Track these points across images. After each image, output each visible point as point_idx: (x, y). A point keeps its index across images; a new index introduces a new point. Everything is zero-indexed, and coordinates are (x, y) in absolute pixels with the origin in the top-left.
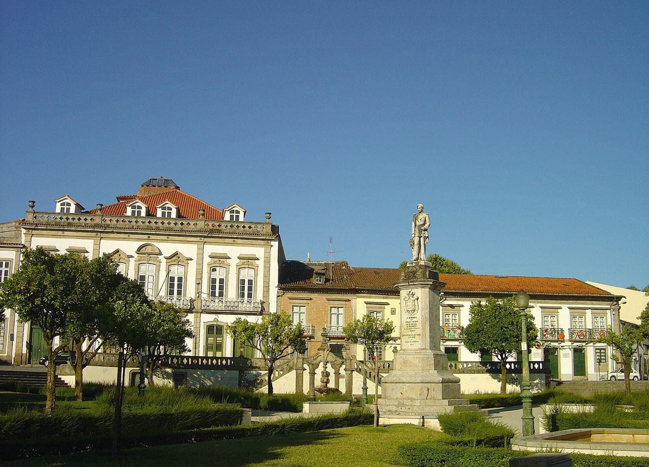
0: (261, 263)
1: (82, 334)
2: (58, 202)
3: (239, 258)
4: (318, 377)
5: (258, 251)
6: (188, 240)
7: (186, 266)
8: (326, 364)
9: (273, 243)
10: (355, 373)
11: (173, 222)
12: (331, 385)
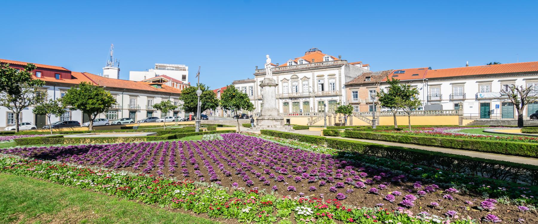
0: (337, 76)
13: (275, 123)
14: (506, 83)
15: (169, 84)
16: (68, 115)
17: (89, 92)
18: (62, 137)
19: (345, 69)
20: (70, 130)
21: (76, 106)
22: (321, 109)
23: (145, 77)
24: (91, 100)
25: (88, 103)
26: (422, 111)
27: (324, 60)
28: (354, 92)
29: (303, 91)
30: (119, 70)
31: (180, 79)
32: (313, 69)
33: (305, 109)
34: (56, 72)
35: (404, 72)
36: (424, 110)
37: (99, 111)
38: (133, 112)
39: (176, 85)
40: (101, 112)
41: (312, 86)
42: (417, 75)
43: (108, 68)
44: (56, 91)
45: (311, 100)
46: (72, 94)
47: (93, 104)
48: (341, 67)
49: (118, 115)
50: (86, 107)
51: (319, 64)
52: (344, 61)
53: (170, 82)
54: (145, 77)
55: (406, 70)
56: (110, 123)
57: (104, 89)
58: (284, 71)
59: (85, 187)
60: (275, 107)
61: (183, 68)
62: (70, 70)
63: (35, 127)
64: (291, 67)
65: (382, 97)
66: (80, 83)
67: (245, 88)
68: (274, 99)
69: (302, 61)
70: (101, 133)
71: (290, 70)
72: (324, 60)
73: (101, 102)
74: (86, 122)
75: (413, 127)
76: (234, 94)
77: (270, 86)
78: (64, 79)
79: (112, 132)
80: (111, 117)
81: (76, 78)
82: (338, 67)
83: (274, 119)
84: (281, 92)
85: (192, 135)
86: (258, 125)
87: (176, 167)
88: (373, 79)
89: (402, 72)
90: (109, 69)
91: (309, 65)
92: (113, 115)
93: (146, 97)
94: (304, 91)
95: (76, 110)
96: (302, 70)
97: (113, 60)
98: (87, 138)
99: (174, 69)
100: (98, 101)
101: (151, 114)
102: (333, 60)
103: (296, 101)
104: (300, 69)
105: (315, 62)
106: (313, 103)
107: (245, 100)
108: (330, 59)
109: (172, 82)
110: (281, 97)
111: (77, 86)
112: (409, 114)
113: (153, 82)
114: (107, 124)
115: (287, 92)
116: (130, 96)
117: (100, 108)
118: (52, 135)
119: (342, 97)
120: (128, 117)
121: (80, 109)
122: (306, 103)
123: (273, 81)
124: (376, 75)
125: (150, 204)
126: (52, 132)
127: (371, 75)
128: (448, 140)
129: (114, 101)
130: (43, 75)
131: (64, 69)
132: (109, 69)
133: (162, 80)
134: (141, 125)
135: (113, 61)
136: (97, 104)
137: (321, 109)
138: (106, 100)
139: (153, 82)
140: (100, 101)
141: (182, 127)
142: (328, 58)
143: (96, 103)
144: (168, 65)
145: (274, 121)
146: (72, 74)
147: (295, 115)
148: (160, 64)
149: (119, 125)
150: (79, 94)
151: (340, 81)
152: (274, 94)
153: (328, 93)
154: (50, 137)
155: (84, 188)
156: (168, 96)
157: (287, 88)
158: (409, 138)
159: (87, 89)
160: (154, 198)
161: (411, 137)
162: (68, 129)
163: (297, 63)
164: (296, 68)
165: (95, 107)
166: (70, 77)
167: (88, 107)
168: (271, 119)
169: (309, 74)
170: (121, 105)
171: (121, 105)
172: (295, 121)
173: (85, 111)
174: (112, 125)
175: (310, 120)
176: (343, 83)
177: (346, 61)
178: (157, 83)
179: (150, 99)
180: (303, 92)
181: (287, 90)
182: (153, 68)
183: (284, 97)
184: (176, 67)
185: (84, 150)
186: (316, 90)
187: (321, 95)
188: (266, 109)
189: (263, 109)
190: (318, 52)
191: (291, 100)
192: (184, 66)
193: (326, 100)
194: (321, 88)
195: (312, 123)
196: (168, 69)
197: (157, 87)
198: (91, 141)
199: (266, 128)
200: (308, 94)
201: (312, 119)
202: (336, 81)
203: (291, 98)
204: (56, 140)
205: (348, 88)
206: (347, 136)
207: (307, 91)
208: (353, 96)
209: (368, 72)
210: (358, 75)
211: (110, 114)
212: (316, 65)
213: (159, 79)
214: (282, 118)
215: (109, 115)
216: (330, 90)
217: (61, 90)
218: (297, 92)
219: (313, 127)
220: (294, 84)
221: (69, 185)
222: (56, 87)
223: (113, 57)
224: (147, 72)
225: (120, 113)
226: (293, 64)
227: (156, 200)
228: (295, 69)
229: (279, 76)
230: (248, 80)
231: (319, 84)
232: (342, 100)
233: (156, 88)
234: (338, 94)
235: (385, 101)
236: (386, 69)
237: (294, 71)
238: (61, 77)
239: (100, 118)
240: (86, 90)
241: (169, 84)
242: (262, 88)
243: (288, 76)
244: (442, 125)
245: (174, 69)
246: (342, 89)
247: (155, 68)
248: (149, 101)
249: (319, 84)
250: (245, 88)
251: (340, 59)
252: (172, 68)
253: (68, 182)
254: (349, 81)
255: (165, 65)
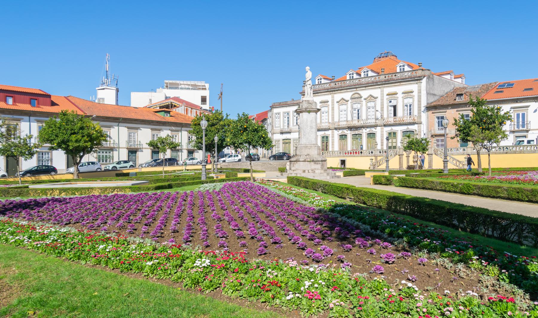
0: (415, 94)
13: (313, 166)
14: (461, 113)
15: (181, 110)
16: (48, 157)
17: (72, 125)
18: (28, 187)
19: (427, 83)
20: (49, 179)
21: (56, 144)
22: (392, 144)
23: (151, 100)
24: (75, 135)
25: (71, 140)
26: (531, 146)
27: (398, 71)
28: (438, 118)
29: (339, 120)
30: (117, 91)
31: (198, 102)
32: (382, 84)
33: (369, 145)
34: (31, 97)
35: (513, 84)
36: (535, 143)
37: (86, 150)
38: (133, 152)
39: (191, 112)
40: (89, 152)
41: (379, 110)
42: (531, 89)
43: (103, 88)
44: (31, 123)
45: (378, 131)
46: (50, 127)
47: (77, 141)
48: (421, 79)
49: (113, 157)
50: (68, 146)
51: (390, 75)
52: (425, 70)
53: (183, 107)
54: (151, 100)
55: (516, 82)
56: (103, 168)
57: (94, 119)
58: (342, 87)
59: (20, 244)
60: (314, 143)
61: (202, 86)
62: (49, 92)
63: (6, 174)
64: (352, 81)
65: (461, 127)
66: (61, 112)
67: (288, 114)
68: (314, 130)
69: (367, 72)
70: (78, 182)
71: (350, 86)
72: (398, 71)
73: (88, 138)
74: (72, 166)
75: (494, 170)
76: (245, 126)
77: (309, 112)
78: (42, 107)
79: (96, 181)
80: (104, 159)
81: (58, 105)
82: (417, 80)
83: (313, 161)
84: (336, 119)
85: (197, 183)
86: (290, 169)
87: (128, 222)
88: (467, 97)
89: (510, 85)
90: (104, 89)
91: (377, 77)
92: (106, 156)
93: (149, 130)
94: (369, 117)
95: (56, 149)
96: (367, 85)
97: (109, 76)
98: (55, 189)
99: (190, 87)
100: (83, 136)
101: (157, 155)
102: (411, 70)
103: (357, 132)
104: (363, 84)
105: (385, 73)
106: (381, 133)
107: (260, 134)
108: (407, 68)
109: (185, 107)
110: (336, 127)
111: (56, 115)
112: (489, 151)
113: (160, 107)
114: (99, 170)
115: (345, 119)
116: (128, 128)
117: (87, 147)
118: (21, 185)
119: (422, 125)
120: (126, 159)
121: (61, 148)
122: (371, 135)
123: (314, 104)
124: (473, 91)
125: (73, 261)
126: (21, 182)
127: (465, 91)
128: (515, 188)
129: (104, 137)
130: (14, 101)
131: (42, 93)
132: (104, 89)
133: (172, 105)
134: (142, 171)
135: (109, 78)
136: (82, 142)
137: (392, 144)
138: (94, 136)
139: (160, 107)
140: (86, 137)
141: (192, 173)
142: (403, 66)
143: (81, 139)
144: (182, 82)
145: (312, 163)
146: (52, 99)
147: (352, 154)
148: (171, 81)
149: (114, 170)
150: (59, 128)
151: (419, 101)
152: (314, 124)
153: (401, 119)
154: (10, 188)
155: (18, 245)
156: (179, 128)
157: (345, 112)
158: (471, 187)
159: (69, 120)
160: (78, 254)
161: (474, 186)
162: (47, 176)
163: (360, 75)
164: (359, 83)
165: (79, 145)
166: (50, 103)
167: (72, 145)
168: (309, 160)
169: (376, 92)
170: (117, 141)
171: (117, 141)
172: (353, 163)
173: (68, 152)
174: (105, 171)
175: (374, 161)
176: (424, 104)
177: (429, 70)
178: (164, 109)
179: (155, 133)
180: (367, 119)
181: (345, 116)
182: (163, 87)
183: (340, 126)
184: (192, 85)
185: (38, 204)
186: (385, 116)
187: (393, 122)
188: (303, 146)
189: (299, 146)
190: (392, 57)
191: (351, 130)
192: (203, 83)
193: (399, 129)
194: (392, 112)
195: (376, 166)
196: (182, 88)
197: (164, 116)
198: (60, 193)
199: (300, 174)
200: (375, 122)
201: (376, 159)
202: (413, 101)
203: (350, 128)
204: (17, 191)
205: (431, 112)
206: (401, 184)
207: (373, 117)
208: (437, 124)
209: (462, 86)
210: (446, 91)
211: (103, 154)
212: (387, 78)
213: (167, 104)
214: (324, 159)
215: (101, 156)
216: (406, 115)
217: (38, 121)
218: (358, 118)
219: (376, 171)
220: (355, 106)
221: (5, 243)
222: (32, 118)
223: (109, 73)
224: (153, 94)
225: (115, 153)
226: (355, 76)
227: (79, 256)
228: (358, 85)
229: (336, 96)
230: (292, 102)
231: (391, 106)
232: (422, 130)
233: (163, 116)
234: (416, 121)
235: (465, 131)
236: (487, 82)
237: (356, 88)
238: (38, 104)
239: (90, 161)
240: (68, 121)
241: (181, 110)
242: (299, 115)
243: (347, 95)
244: (510, 167)
245: (190, 87)
246: (422, 113)
247: (165, 87)
248: (154, 135)
249: (391, 106)
250: (288, 114)
251: (421, 68)
252: (187, 87)
253: (4, 239)
254: (432, 101)
255: (178, 82)
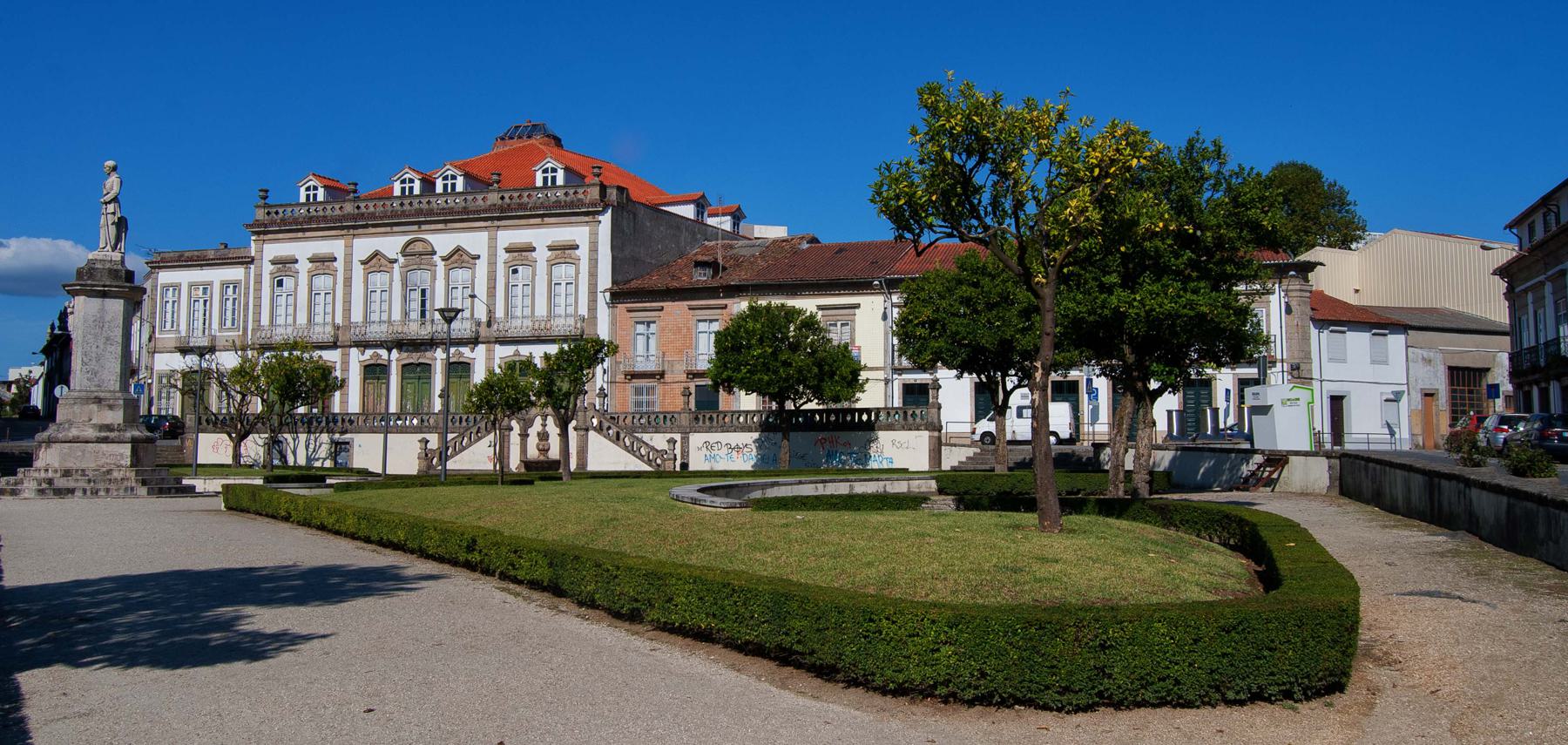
0: (583, 253)
1: (20, 392)
2: (396, 181)
3: (551, 248)
4: (533, 441)
5: (577, 233)
6: (531, 223)
7: (472, 267)
8: (546, 420)
9: (601, 218)
10: (592, 434)
11: (320, 208)
12: (554, 453)
